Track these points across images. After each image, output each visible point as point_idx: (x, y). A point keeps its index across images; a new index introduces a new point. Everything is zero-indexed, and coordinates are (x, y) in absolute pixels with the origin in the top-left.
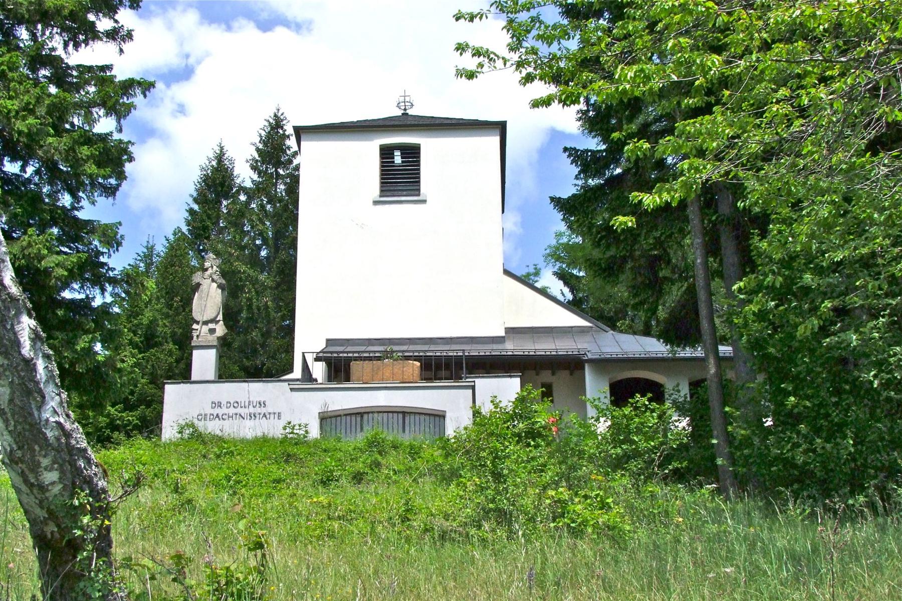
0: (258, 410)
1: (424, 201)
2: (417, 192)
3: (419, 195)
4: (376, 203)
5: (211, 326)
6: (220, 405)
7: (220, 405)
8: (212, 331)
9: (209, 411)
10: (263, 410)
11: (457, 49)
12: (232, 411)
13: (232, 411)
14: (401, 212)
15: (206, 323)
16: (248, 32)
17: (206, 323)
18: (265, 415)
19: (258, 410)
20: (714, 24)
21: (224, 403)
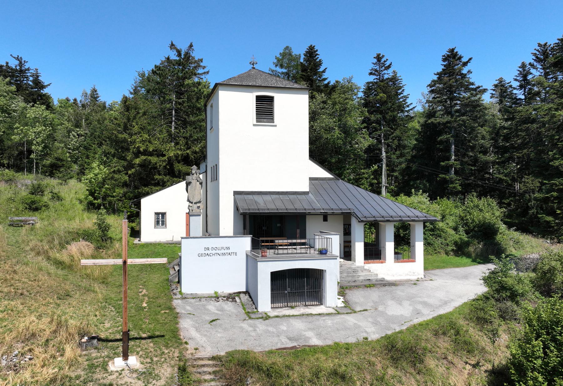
0: (226, 251)
1: (276, 126)
2: (272, 120)
3: (274, 122)
4: (254, 125)
5: (198, 205)
6: (208, 249)
7: (208, 249)
8: (199, 207)
9: (203, 252)
10: (228, 251)
11: (378, 55)
12: (214, 252)
13: (214, 252)
14: (265, 130)
15: (196, 203)
16: (469, 64)
17: (196, 203)
18: (229, 254)
19: (226, 251)
20: (525, 90)
21: (210, 248)
